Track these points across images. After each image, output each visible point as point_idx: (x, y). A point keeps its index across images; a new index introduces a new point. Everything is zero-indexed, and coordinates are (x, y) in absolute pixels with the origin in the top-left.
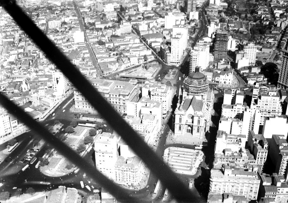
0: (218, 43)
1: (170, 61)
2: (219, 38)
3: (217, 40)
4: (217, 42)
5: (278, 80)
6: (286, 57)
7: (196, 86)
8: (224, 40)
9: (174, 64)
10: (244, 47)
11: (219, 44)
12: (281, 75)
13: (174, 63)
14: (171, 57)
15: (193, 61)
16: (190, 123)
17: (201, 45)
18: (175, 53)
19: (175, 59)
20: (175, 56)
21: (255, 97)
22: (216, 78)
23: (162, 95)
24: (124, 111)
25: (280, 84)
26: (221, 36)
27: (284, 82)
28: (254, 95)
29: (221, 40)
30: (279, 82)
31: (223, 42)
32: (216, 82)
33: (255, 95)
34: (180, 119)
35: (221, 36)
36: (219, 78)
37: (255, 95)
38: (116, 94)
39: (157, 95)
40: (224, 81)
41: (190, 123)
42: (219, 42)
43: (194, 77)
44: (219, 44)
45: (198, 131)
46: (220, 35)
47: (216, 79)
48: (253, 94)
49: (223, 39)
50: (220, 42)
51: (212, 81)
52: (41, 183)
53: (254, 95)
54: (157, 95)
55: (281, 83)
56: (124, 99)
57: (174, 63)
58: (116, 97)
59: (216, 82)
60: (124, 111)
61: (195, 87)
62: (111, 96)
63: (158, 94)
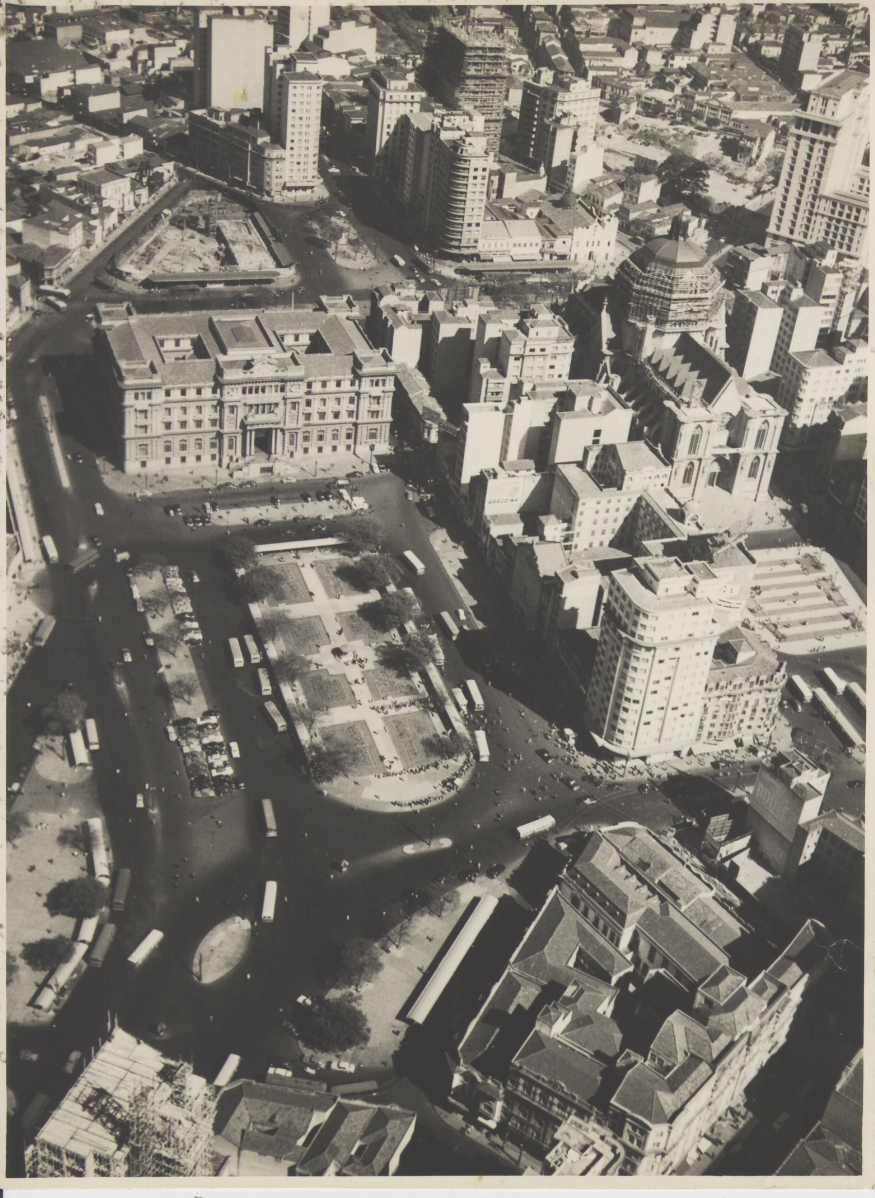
0: (472, 88)
1: (279, 180)
2: (475, 64)
3: (469, 73)
4: (468, 82)
5: (767, 225)
6: (806, 138)
7: (693, 296)
8: (493, 73)
9: (300, 193)
10: (559, 98)
11: (474, 92)
12: (783, 205)
13: (297, 188)
14: (287, 165)
15: (471, 179)
16: (721, 447)
17: (402, 99)
18: (304, 145)
19: (302, 174)
20: (302, 160)
21: (827, 305)
22: (558, 242)
23: (560, 351)
24: (144, 464)
25: (776, 237)
26: (481, 57)
27: (797, 229)
28: (824, 297)
29: (481, 73)
30: (772, 229)
31: (492, 82)
32: (555, 258)
33: (828, 297)
34: (695, 440)
35: (481, 57)
36: (568, 239)
37: (828, 297)
38: (325, 378)
39: (538, 352)
40: (590, 249)
41: (721, 447)
42: (473, 82)
43: (679, 260)
44: (474, 92)
45: (752, 474)
46: (480, 52)
47: (559, 247)
48: (824, 293)
49: (491, 67)
50: (478, 82)
51: (542, 253)
52: (409, 849)
53: (824, 297)
54: (538, 352)
55: (784, 232)
56: (146, 407)
57: (297, 188)
58: (342, 389)
59: (555, 258)
60: (144, 464)
61: (691, 300)
62: (317, 387)
63: (543, 350)
